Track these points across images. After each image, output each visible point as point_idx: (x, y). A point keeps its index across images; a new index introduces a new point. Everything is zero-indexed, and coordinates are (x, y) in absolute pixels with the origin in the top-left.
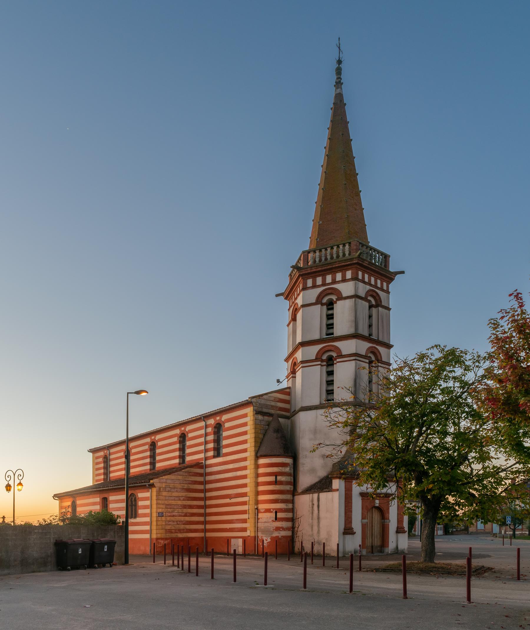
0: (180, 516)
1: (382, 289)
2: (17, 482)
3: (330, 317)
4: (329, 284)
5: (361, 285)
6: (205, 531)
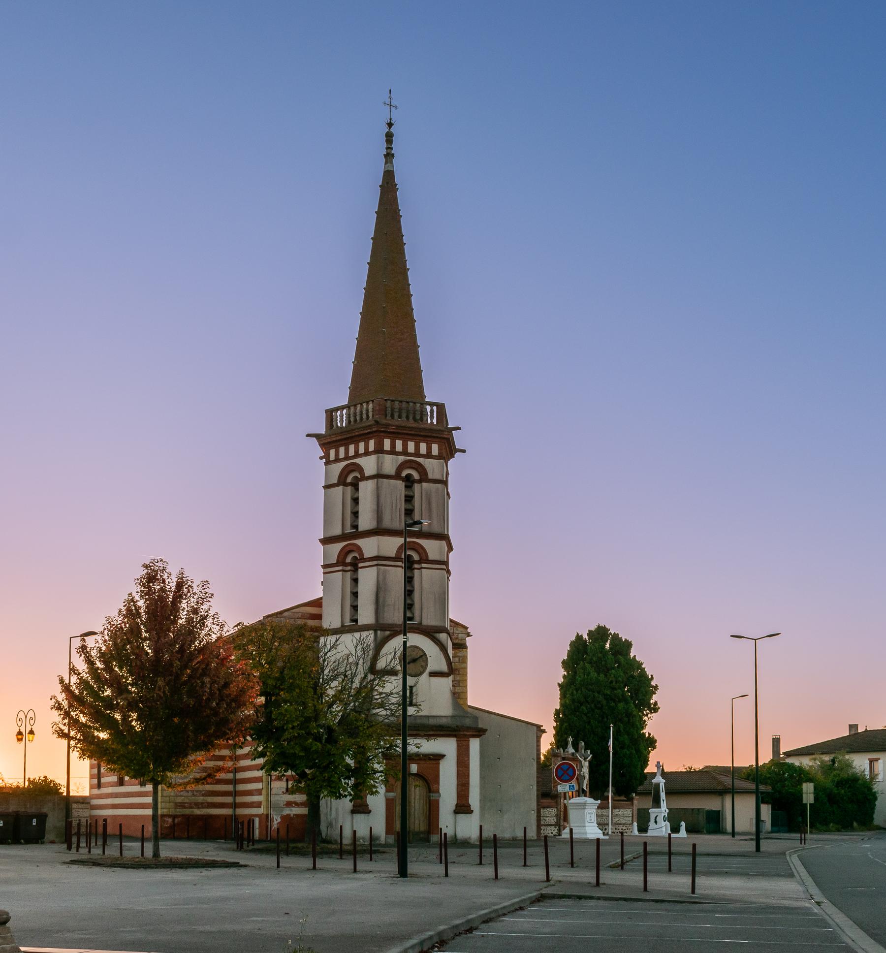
2: (28, 729)
3: (409, 499)
6: (235, 806)
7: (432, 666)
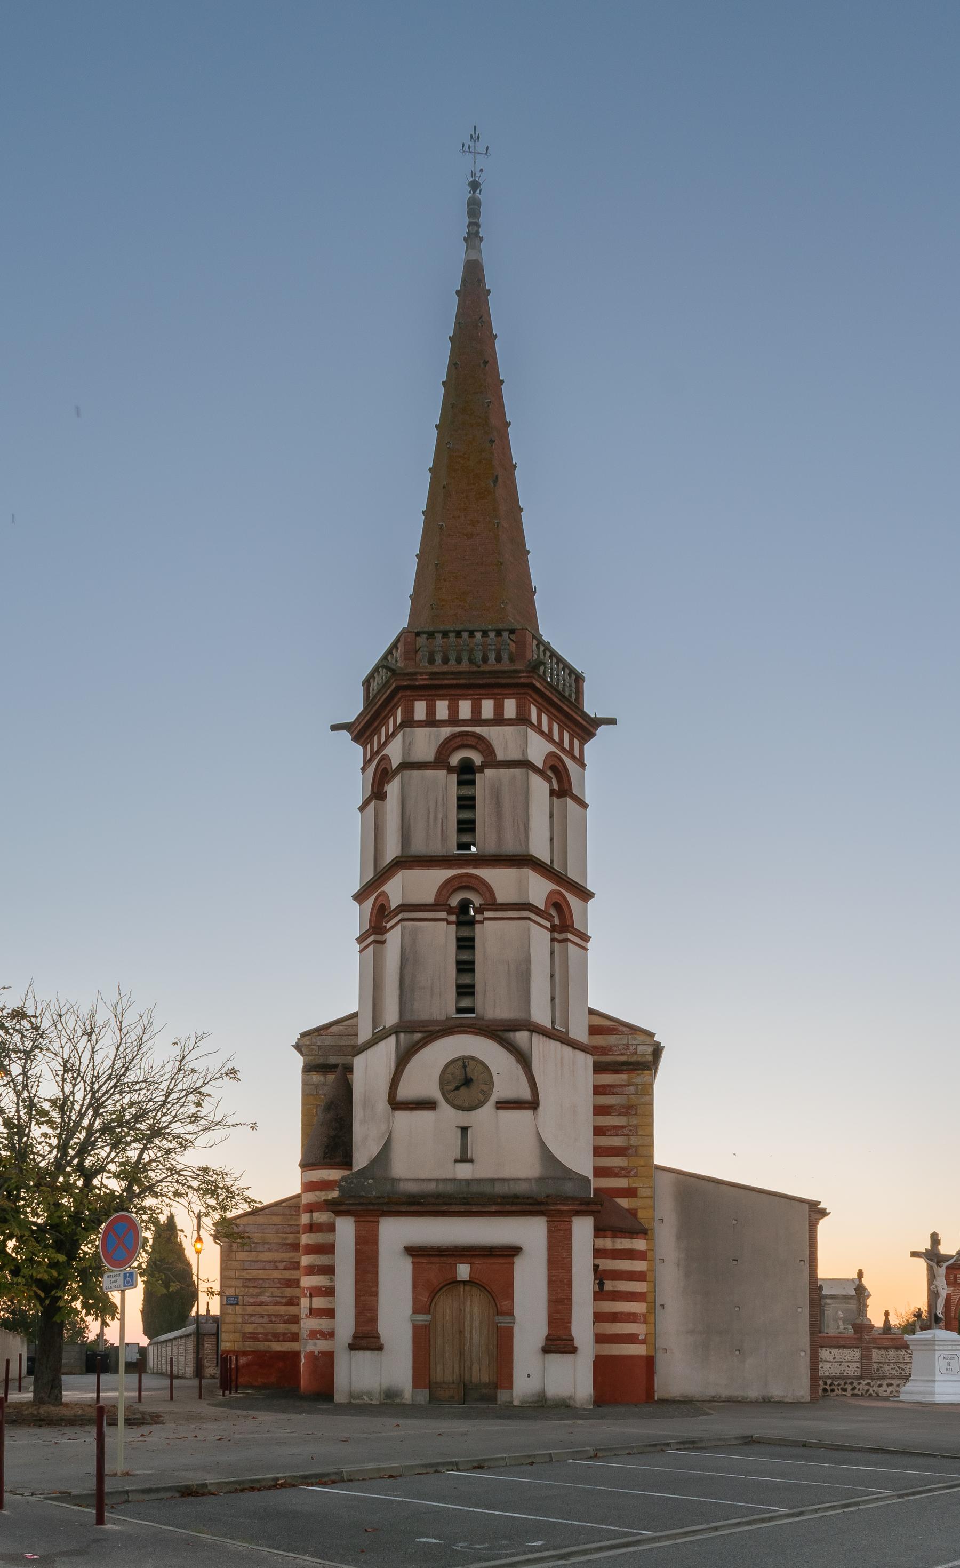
0: (277, 1304)
1: (571, 754)
3: (466, 803)
4: (465, 723)
5: (533, 736)
7: (501, 1090)
